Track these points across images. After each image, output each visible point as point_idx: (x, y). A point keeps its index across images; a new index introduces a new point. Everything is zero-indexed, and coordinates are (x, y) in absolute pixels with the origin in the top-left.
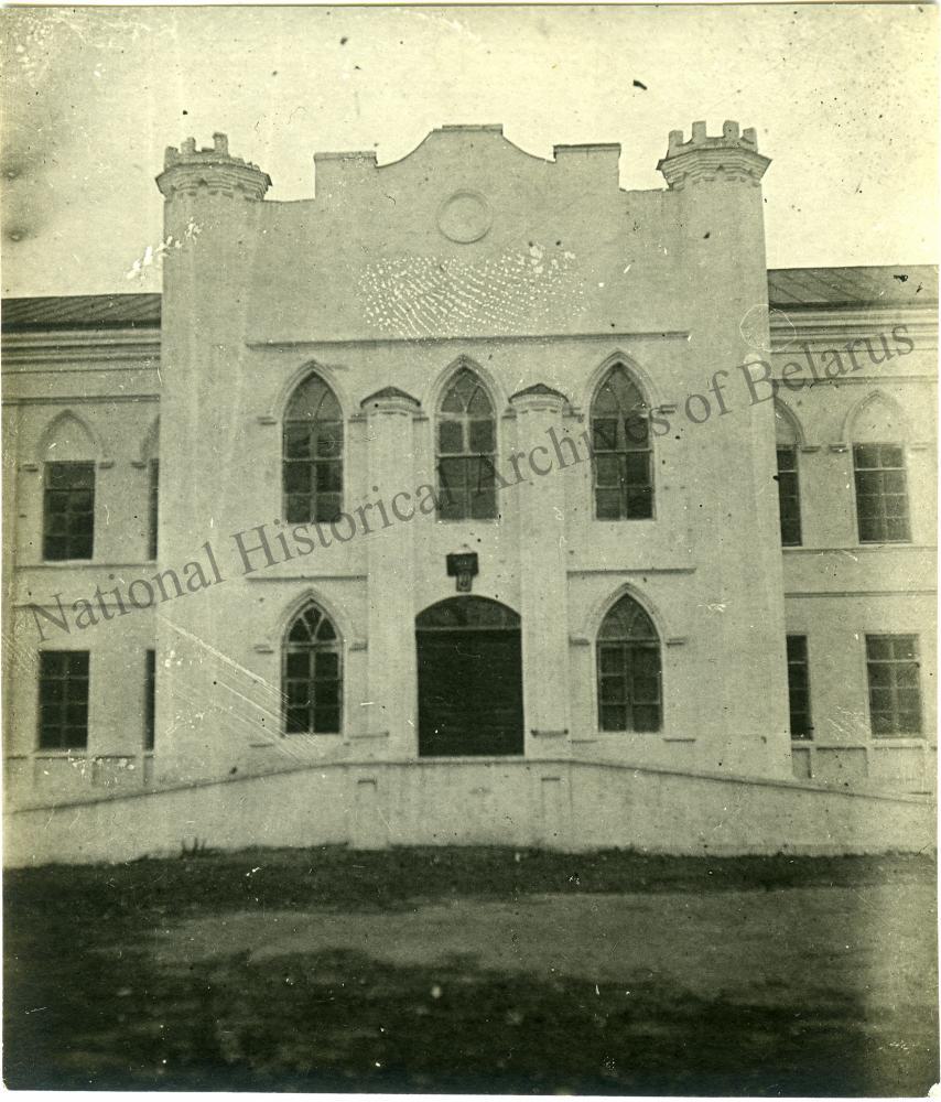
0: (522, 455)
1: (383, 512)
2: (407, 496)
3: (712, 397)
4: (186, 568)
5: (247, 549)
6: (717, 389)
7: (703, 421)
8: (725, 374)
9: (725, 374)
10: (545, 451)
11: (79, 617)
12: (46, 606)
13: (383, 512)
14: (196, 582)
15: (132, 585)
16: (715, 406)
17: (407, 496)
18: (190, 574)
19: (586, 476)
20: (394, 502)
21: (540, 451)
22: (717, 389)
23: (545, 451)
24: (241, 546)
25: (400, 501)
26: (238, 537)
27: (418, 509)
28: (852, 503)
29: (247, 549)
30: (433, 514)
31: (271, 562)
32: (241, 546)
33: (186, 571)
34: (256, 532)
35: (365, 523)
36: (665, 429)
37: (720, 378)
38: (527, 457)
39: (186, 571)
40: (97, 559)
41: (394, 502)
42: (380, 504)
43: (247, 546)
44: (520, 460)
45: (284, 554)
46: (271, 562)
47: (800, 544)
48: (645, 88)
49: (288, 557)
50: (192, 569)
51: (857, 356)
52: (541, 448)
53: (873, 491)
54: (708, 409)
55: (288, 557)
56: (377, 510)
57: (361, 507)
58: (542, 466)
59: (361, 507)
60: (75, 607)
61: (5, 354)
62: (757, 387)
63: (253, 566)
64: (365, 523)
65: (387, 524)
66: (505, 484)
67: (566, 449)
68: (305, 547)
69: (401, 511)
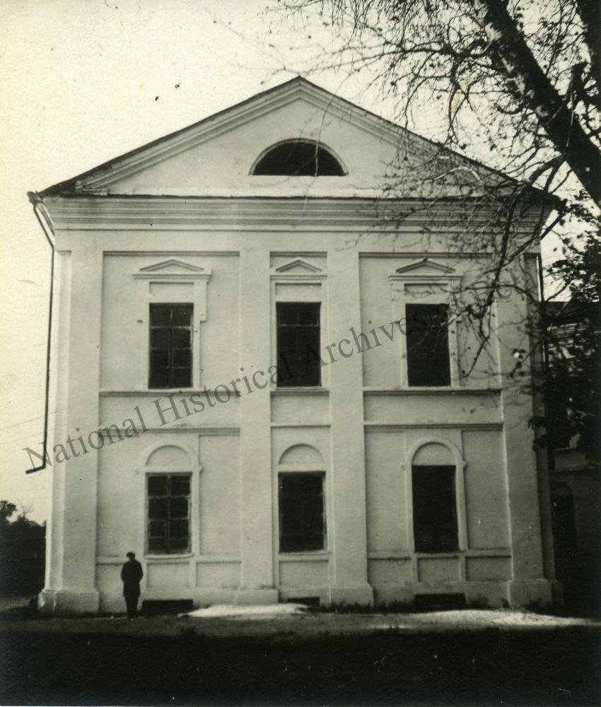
2: (262, 373)
4: (124, 423)
10: (348, 342)
15: (90, 435)
16: (251, 382)
17: (262, 373)
20: (254, 376)
21: (345, 342)
23: (348, 342)
25: (258, 376)
27: (269, 380)
28: (312, 135)
30: (109, 428)
31: (178, 417)
38: (337, 346)
40: (196, 387)
41: (254, 376)
42: (245, 379)
43: (162, 408)
44: (332, 349)
45: (174, 416)
46: (178, 417)
48: (28, 472)
49: (189, 414)
52: (346, 340)
54: (254, 378)
55: (189, 414)
56: (243, 382)
57: (233, 381)
58: (347, 352)
59: (233, 381)
60: (358, 61)
63: (166, 420)
65: (250, 391)
66: (325, 364)
68: (199, 407)
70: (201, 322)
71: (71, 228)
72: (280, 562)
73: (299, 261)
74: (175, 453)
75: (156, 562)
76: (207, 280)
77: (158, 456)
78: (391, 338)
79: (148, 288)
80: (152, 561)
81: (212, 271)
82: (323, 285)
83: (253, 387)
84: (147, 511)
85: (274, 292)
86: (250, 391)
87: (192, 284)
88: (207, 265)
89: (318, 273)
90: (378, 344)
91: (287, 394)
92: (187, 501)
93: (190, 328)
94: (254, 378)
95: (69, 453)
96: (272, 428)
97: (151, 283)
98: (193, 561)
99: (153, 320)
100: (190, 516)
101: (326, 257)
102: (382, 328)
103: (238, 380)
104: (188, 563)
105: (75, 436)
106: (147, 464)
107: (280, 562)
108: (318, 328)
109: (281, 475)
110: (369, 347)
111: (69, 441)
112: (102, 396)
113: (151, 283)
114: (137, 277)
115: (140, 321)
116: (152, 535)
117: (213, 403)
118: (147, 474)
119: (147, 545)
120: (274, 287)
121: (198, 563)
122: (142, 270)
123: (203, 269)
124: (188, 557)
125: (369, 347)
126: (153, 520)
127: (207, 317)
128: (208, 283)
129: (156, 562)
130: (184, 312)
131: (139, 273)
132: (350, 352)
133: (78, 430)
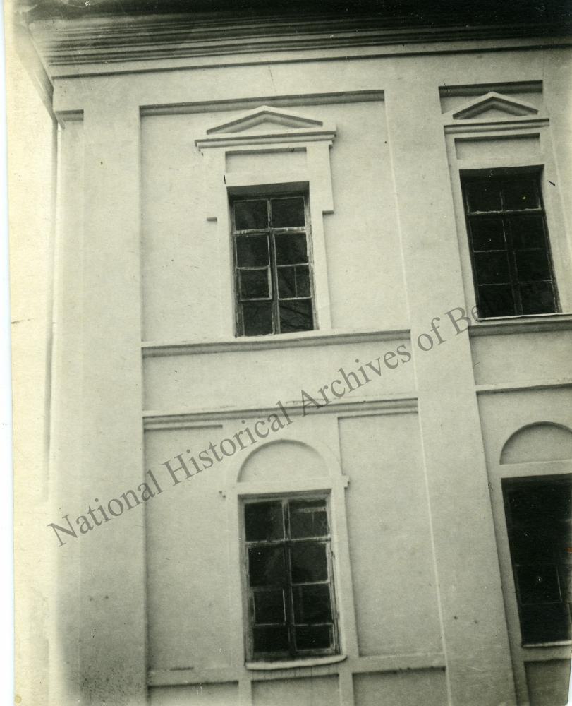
0: (326, 387)
1: (250, 435)
3: (433, 334)
5: (173, 470)
6: (435, 329)
7: (226, 440)
8: (438, 319)
9: (438, 319)
10: (339, 382)
11: (273, 425)
12: (318, 399)
13: (250, 435)
14: (85, 528)
16: (435, 339)
18: (81, 524)
19: (205, 338)
22: (435, 329)
23: (339, 382)
24: (169, 469)
26: (167, 464)
29: (173, 470)
32: (169, 469)
33: (78, 522)
34: (177, 459)
35: (241, 444)
36: (201, 456)
37: (435, 321)
39: (78, 522)
40: (324, 323)
42: (247, 430)
47: (311, 328)
49: (199, 471)
50: (81, 521)
51: (322, 397)
53: (30, 11)
54: (122, 509)
55: (199, 471)
61: (382, 98)
62: (458, 323)
64: (241, 444)
67: (351, 378)
69: (262, 433)
70: (325, 214)
71: (81, 72)
72: (527, 664)
73: (493, 99)
74: (289, 453)
75: (268, 677)
76: (330, 142)
77: (260, 462)
78: (379, 373)
79: (224, 162)
80: (261, 677)
81: (337, 128)
82: (541, 137)
83: (109, 515)
84: (246, 572)
85: (454, 151)
86: (107, 519)
87: (304, 150)
88: (330, 118)
89: (531, 117)
90: (368, 380)
91: (500, 332)
92: (323, 548)
93: (305, 229)
94: (122, 509)
95: (92, 523)
96: (479, 394)
97: (228, 154)
98: (345, 673)
99: (238, 221)
100: (333, 577)
101: (540, 91)
102: (369, 365)
103: (241, 433)
104: (337, 675)
105: (95, 506)
106: (240, 478)
107: (527, 664)
108: (543, 214)
109: (506, 483)
110: (152, 495)
111: (91, 512)
112: (151, 354)
113: (228, 154)
114: (201, 145)
115: (213, 220)
116: (258, 620)
117: (99, 522)
118: (242, 498)
119: (250, 641)
120: (452, 144)
121: (355, 675)
122: (209, 132)
123: (320, 124)
124: (337, 663)
125: (152, 495)
126: (256, 589)
127: (335, 205)
128: (330, 147)
129: (268, 677)
130: (291, 201)
131: (205, 137)
132: (266, 433)
133: (97, 500)
